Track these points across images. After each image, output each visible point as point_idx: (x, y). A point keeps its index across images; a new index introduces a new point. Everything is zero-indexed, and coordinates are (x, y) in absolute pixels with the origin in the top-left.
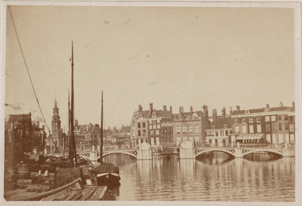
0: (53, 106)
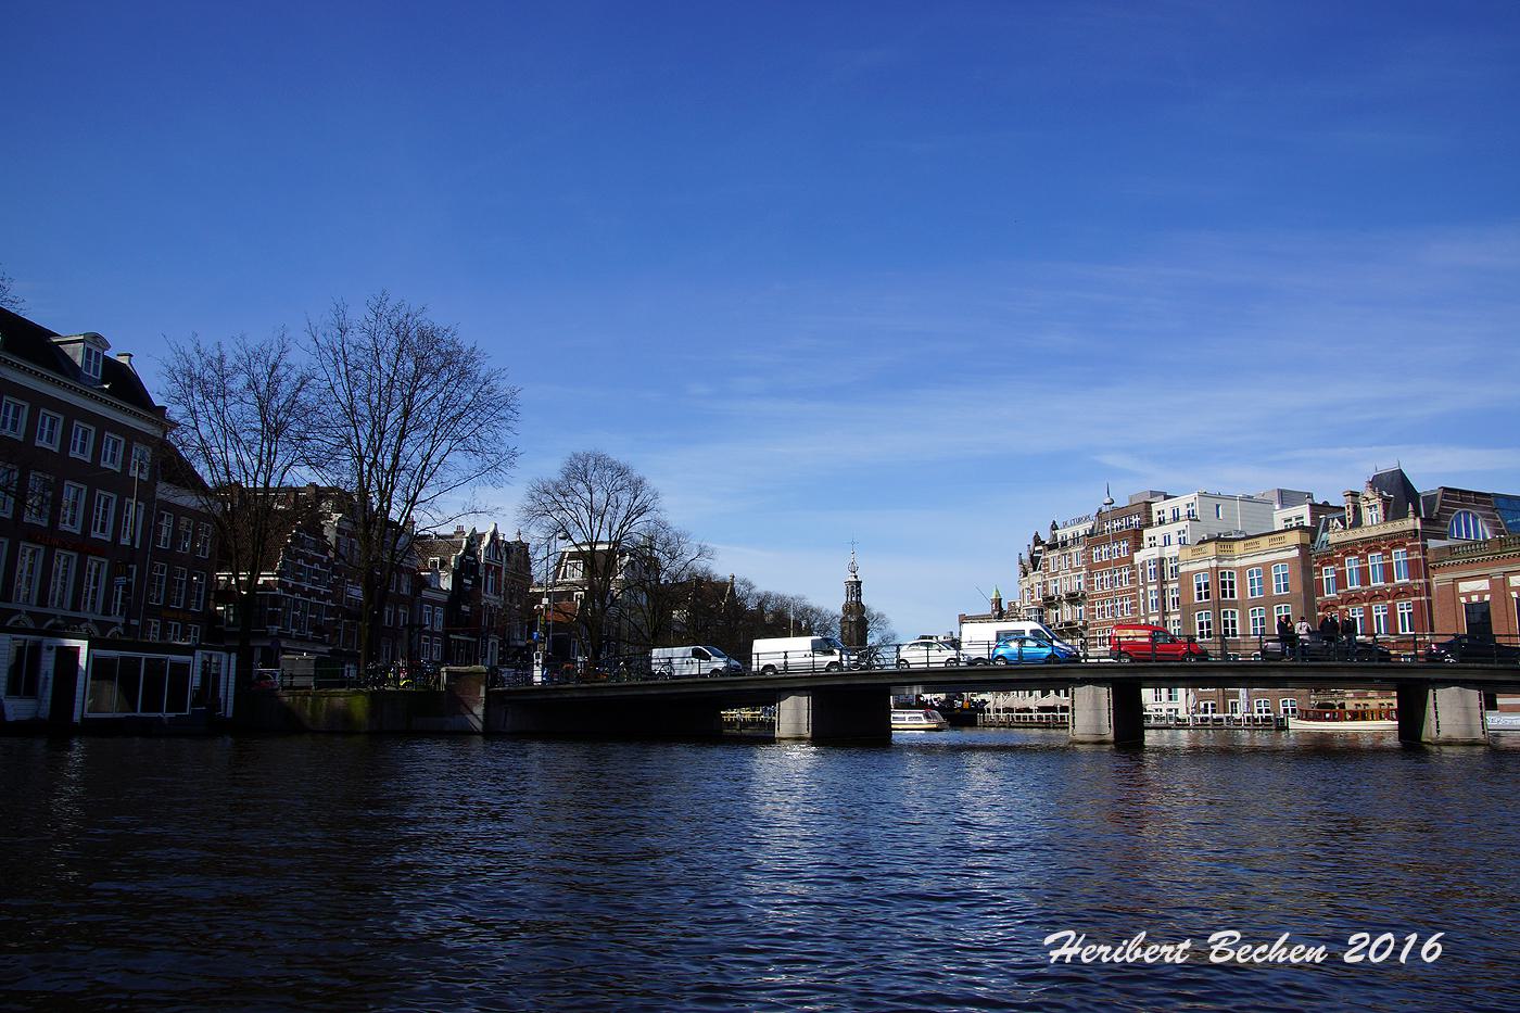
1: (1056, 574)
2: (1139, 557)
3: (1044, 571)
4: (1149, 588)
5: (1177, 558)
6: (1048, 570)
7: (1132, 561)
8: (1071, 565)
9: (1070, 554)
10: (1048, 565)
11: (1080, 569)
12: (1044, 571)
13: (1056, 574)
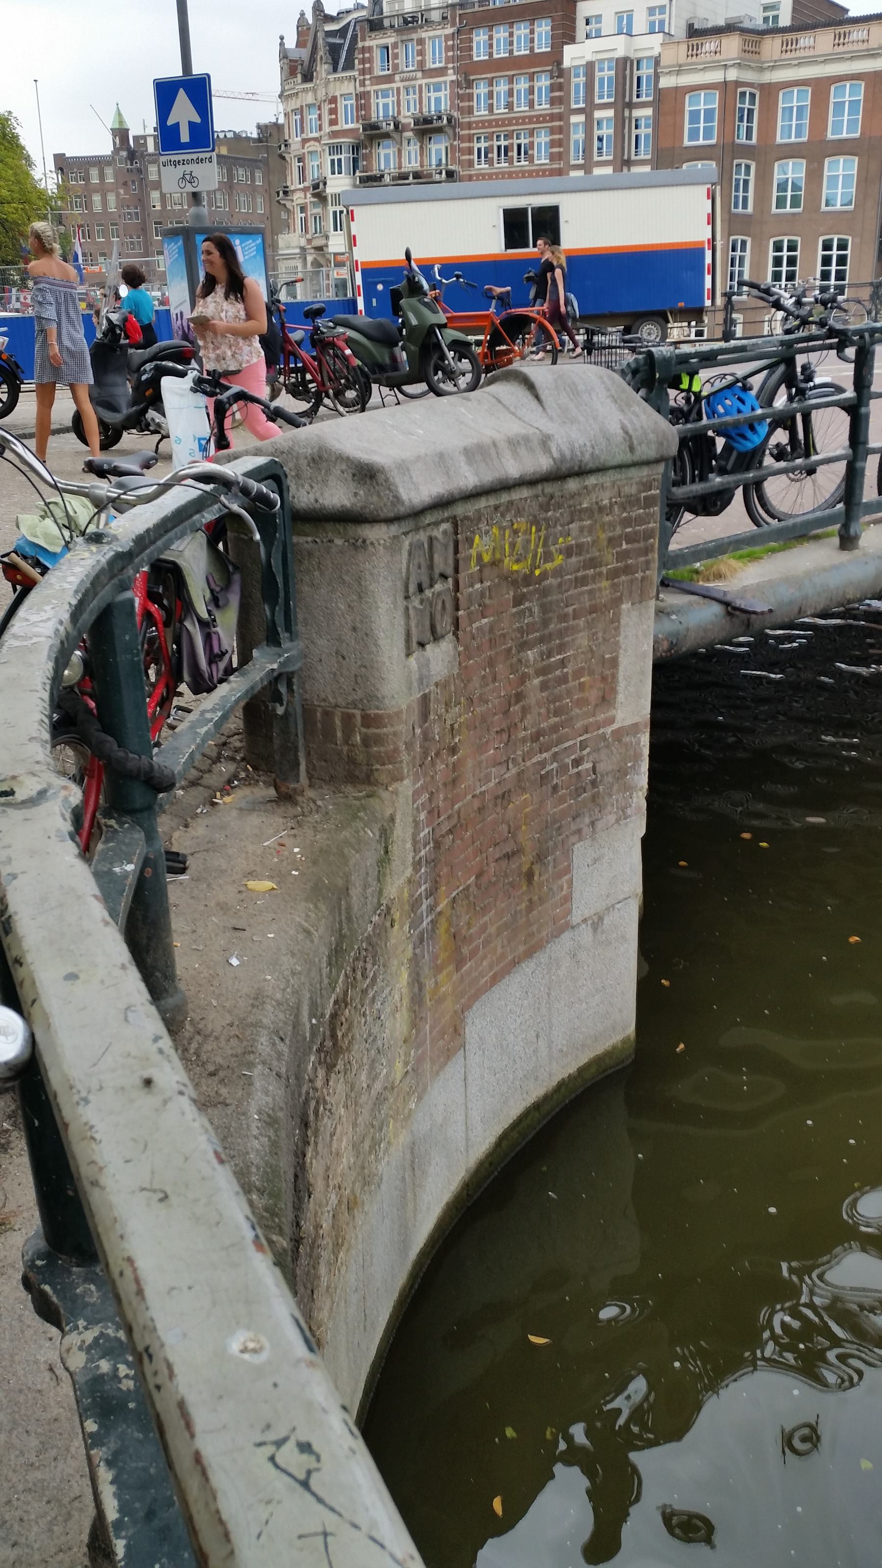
2: (572, 55)
3: (363, 72)
4: (598, 114)
5: (657, 61)
6: (370, 71)
7: (560, 62)
8: (422, 63)
9: (421, 42)
11: (442, 71)
12: (363, 72)
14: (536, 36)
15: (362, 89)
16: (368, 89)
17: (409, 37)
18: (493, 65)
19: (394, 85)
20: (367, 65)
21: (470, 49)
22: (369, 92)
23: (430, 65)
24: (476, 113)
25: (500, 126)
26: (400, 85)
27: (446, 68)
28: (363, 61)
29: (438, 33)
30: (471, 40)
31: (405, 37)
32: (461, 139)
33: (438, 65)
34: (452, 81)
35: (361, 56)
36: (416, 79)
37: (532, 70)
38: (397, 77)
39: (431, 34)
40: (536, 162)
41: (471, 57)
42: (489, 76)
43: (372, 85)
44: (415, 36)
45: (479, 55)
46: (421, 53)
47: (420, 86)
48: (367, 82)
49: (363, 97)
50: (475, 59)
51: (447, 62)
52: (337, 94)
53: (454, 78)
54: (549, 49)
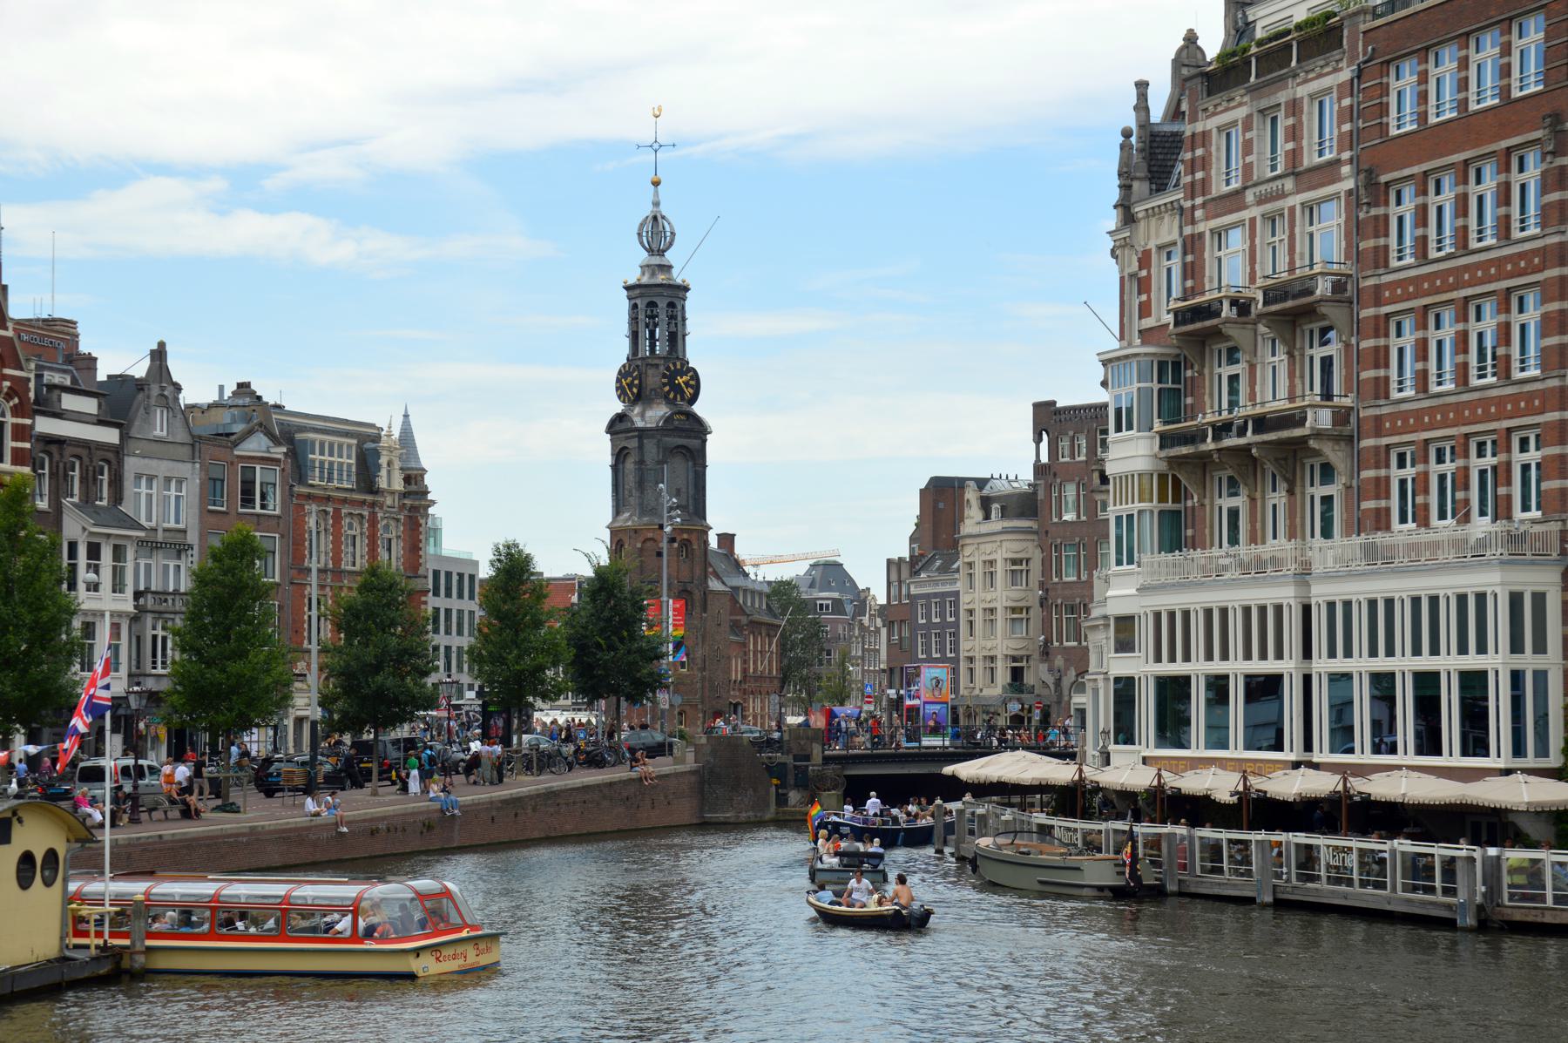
0: (631, 264)
1: (1234, 201)
3: (1192, 190)
6: (1205, 184)
8: (1294, 156)
9: (1294, 107)
10: (1205, 163)
11: (1328, 172)
12: (1192, 190)
13: (1234, 201)
14: (1515, 60)
15: (1188, 230)
16: (1201, 227)
17: (1272, 101)
18: (1430, 138)
19: (1245, 215)
20: (1199, 175)
21: (1383, 109)
22: (1201, 235)
23: (1310, 159)
24: (1394, 263)
25: (1482, 282)
26: (1255, 212)
27: (1337, 163)
28: (1192, 167)
29: (1327, 82)
30: (1385, 90)
31: (1264, 103)
32: (1359, 328)
33: (1328, 156)
34: (1349, 193)
35: (1188, 156)
36: (1282, 195)
37: (1504, 144)
38: (1250, 196)
39: (1314, 86)
40: (1434, 389)
41: (1384, 128)
42: (1416, 170)
43: (1207, 218)
44: (1282, 97)
45: (1401, 122)
46: (1294, 134)
47: (1292, 210)
48: (1199, 214)
49: (1192, 244)
50: (1394, 132)
51: (1340, 151)
52: (1152, 245)
53: (1349, 184)
54: (1455, 114)
